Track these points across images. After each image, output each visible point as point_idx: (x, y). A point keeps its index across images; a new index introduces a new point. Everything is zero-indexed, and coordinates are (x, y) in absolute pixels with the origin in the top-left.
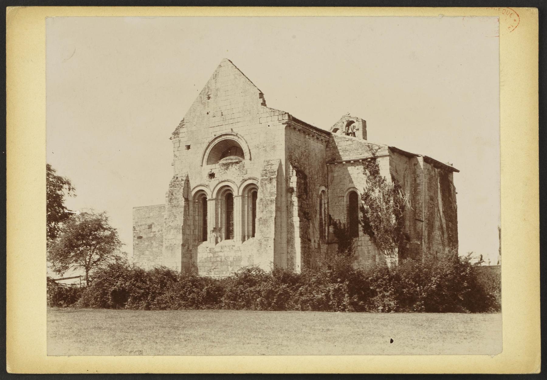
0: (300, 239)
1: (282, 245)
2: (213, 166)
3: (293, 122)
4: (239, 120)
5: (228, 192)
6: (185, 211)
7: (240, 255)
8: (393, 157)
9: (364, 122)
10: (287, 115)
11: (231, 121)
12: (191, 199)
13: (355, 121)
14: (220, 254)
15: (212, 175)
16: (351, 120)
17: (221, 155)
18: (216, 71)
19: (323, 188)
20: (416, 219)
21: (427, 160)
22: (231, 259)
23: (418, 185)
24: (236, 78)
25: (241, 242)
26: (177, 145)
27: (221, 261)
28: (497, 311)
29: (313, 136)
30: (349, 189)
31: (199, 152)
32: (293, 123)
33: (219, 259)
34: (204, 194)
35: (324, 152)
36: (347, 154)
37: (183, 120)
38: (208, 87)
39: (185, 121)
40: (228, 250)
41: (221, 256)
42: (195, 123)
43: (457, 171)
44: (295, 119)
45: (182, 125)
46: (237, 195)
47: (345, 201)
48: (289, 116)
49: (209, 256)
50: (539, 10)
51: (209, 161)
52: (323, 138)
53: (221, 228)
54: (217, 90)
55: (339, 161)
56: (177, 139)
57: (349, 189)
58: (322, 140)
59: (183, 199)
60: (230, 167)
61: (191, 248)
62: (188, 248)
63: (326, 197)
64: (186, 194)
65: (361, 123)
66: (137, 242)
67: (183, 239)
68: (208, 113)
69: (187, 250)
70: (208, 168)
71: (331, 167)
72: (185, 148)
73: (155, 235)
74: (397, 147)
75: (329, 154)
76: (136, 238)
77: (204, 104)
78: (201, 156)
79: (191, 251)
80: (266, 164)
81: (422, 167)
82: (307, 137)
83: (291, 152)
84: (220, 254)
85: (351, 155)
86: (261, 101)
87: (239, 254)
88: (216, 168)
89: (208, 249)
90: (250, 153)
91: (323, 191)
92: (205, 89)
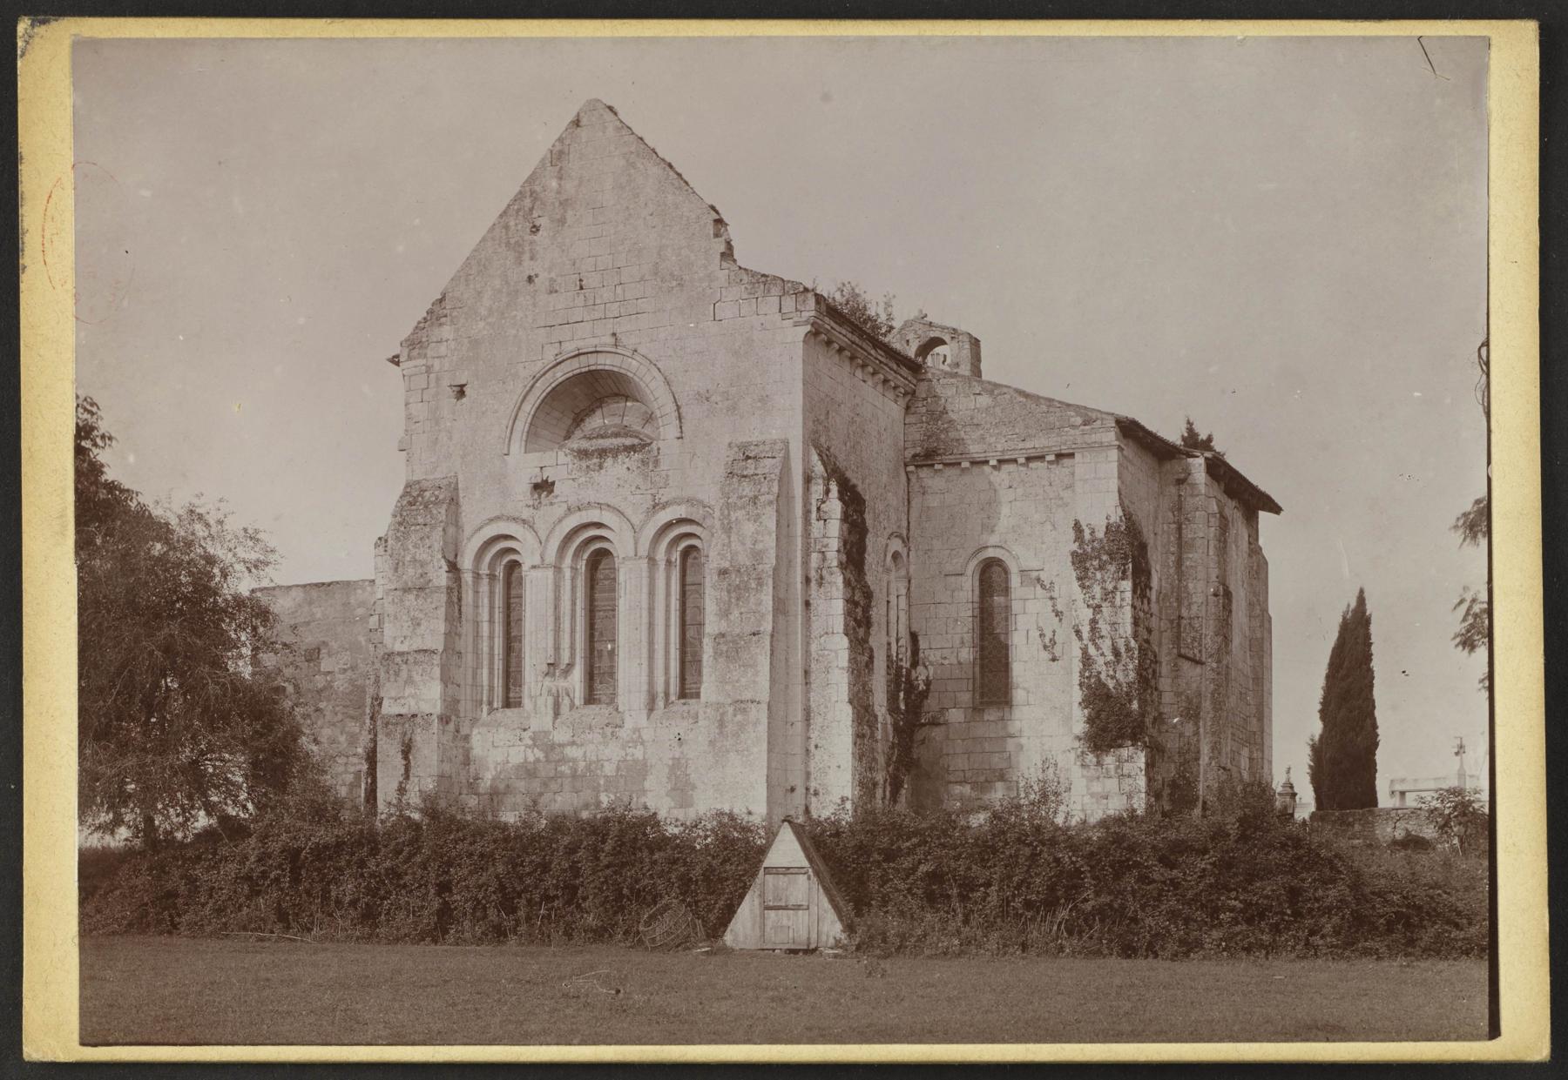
2: (548, 458)
5: (598, 545)
6: (449, 603)
9: (975, 343)
10: (811, 297)
12: (466, 563)
13: (947, 338)
14: (571, 752)
15: (543, 487)
16: (932, 334)
17: (569, 422)
18: (560, 140)
20: (1180, 655)
22: (609, 769)
25: (645, 712)
27: (574, 776)
31: (505, 401)
32: (828, 323)
33: (565, 769)
34: (513, 551)
37: (441, 301)
39: (448, 304)
40: (598, 737)
41: (574, 760)
43: (1275, 509)
46: (537, 561)
47: (968, 587)
48: (819, 299)
50: (1541, 28)
51: (533, 437)
53: (571, 666)
54: (564, 204)
55: (948, 459)
56: (421, 362)
59: (443, 563)
60: (609, 461)
61: (464, 731)
63: (903, 572)
65: (967, 346)
68: (530, 279)
69: (455, 738)
70: (525, 466)
71: (918, 478)
73: (329, 686)
75: (917, 436)
77: (517, 248)
79: (467, 738)
81: (1203, 489)
82: (859, 373)
87: (638, 753)
88: (558, 463)
89: (526, 735)
90: (680, 418)
92: (520, 196)
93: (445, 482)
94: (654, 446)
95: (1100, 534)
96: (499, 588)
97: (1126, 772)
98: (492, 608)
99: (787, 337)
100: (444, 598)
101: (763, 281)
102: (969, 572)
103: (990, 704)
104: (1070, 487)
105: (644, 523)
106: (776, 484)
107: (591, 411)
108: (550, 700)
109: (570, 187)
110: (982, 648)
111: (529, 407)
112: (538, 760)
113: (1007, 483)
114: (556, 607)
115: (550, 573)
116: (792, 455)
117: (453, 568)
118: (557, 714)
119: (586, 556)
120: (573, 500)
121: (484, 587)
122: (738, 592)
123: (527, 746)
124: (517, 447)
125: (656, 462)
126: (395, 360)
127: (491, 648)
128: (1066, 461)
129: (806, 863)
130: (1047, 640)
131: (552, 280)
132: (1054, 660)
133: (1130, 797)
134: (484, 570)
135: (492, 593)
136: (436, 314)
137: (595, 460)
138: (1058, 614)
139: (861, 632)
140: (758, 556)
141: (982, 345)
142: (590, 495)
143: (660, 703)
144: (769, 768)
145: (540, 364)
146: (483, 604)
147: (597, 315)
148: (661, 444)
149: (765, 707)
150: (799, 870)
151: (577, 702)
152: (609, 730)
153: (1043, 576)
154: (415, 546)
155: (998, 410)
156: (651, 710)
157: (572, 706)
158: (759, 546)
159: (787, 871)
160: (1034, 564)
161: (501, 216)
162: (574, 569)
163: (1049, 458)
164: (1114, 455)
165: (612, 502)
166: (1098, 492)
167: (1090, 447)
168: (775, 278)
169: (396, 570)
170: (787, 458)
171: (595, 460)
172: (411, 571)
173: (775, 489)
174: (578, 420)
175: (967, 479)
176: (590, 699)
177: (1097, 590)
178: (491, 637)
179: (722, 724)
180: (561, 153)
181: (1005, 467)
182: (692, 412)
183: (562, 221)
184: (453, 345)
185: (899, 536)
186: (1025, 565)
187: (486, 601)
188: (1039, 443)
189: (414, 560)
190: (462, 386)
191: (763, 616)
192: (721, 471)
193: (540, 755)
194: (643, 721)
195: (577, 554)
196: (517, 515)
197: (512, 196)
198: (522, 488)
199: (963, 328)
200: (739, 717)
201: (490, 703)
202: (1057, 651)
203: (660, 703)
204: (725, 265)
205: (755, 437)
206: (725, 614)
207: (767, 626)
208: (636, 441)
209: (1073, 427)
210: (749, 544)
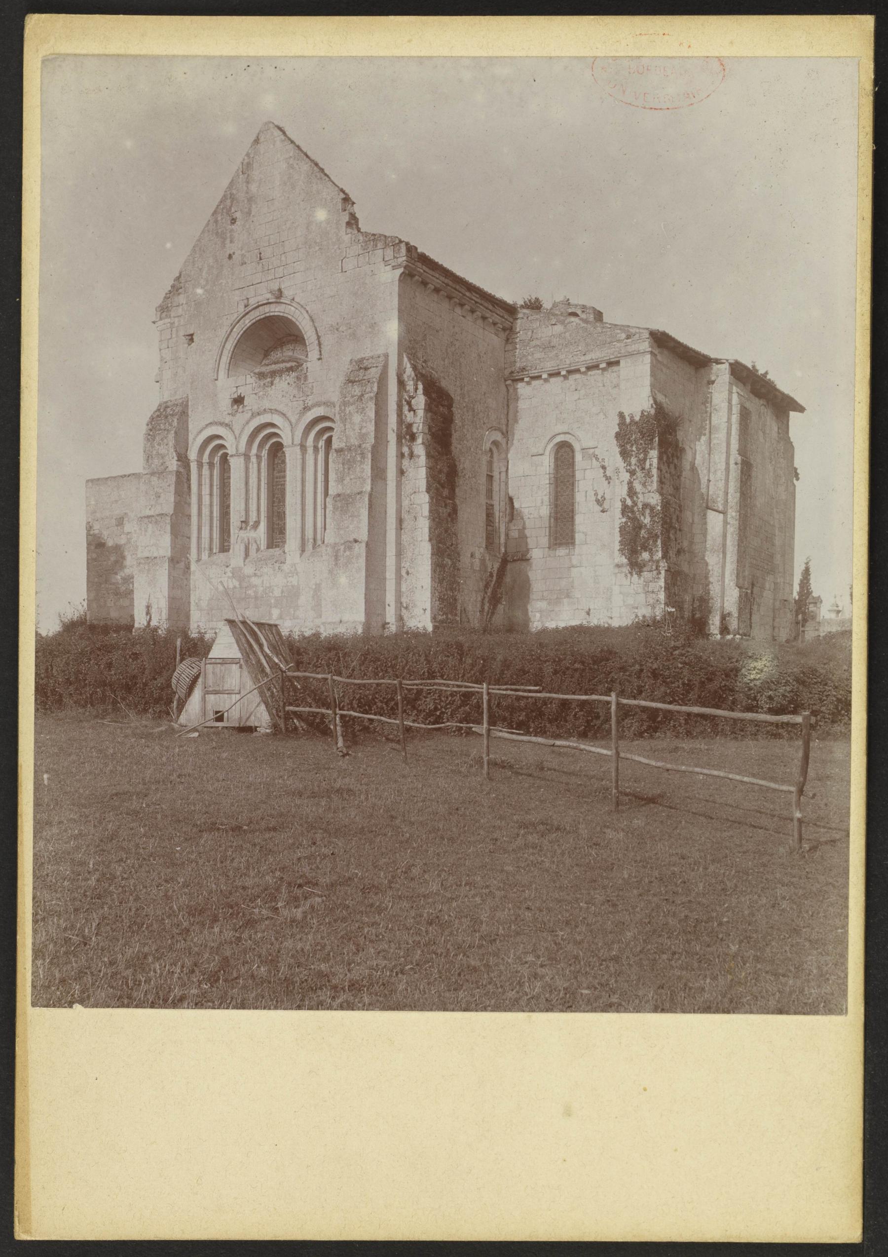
3: (419, 265)
5: (275, 440)
8: (659, 357)
10: (403, 246)
12: (193, 455)
14: (255, 581)
15: (238, 401)
18: (248, 155)
21: (743, 375)
22: (277, 593)
24: (291, 167)
25: (299, 552)
27: (256, 598)
28: (133, 578)
30: (554, 436)
32: (421, 268)
33: (251, 592)
36: (551, 355)
38: (231, 194)
39: (182, 280)
41: (256, 586)
43: (801, 409)
44: (424, 259)
48: (410, 249)
52: (497, 319)
53: (257, 524)
54: (250, 200)
56: (169, 320)
57: (554, 436)
58: (495, 324)
59: (174, 454)
60: (277, 380)
66: (94, 556)
68: (230, 257)
70: (227, 386)
72: (184, 340)
76: (93, 547)
82: (458, 310)
84: (255, 581)
85: (562, 357)
86: (346, 218)
87: (294, 581)
88: (245, 382)
89: (229, 569)
90: (320, 344)
91: (495, 443)
93: (181, 401)
94: (304, 366)
95: (637, 418)
96: (216, 472)
97: (650, 589)
98: (211, 486)
99: (388, 277)
100: (174, 479)
101: (374, 239)
102: (547, 453)
103: (560, 545)
104: (617, 386)
105: (299, 420)
106: (376, 385)
107: (274, 348)
108: (243, 548)
109: (253, 188)
110: (556, 506)
111: (230, 346)
112: (235, 587)
113: (573, 387)
114: (247, 483)
115: (242, 459)
116: (390, 366)
117: (183, 458)
118: (247, 555)
119: (267, 447)
120: (255, 408)
121: (206, 471)
122: (349, 464)
123: (229, 577)
124: (222, 374)
125: (306, 378)
126: (154, 322)
127: (211, 512)
128: (615, 368)
129: (239, 655)
130: (599, 497)
131: (243, 256)
132: (603, 511)
133: (653, 607)
134: (206, 458)
135: (211, 476)
136: (176, 289)
137: (269, 380)
138: (608, 479)
139: (446, 492)
140: (363, 437)
141: (604, 315)
142: (267, 404)
143: (310, 546)
144: (366, 588)
145: (236, 315)
146: (203, 485)
147: (270, 278)
148: (309, 364)
149: (364, 545)
150: (233, 661)
151: (262, 548)
152: (277, 565)
153: (597, 452)
154: (159, 444)
155: (567, 334)
156: (303, 551)
157: (258, 550)
158: (364, 431)
159: (224, 662)
160: (591, 444)
161: (213, 215)
162: (259, 457)
163: (603, 365)
164: (648, 358)
165: (281, 408)
166: (635, 390)
167: (631, 355)
168: (381, 235)
169: (148, 461)
170: (385, 367)
171: (269, 380)
172: (156, 461)
173: (375, 389)
174: (266, 354)
175: (547, 386)
176: (271, 545)
177: (634, 460)
178: (211, 505)
179: (336, 558)
180: (249, 164)
181: (572, 377)
182: (328, 341)
183: (249, 213)
184: (185, 307)
185: (499, 430)
186: (585, 445)
187: (208, 481)
188: (595, 355)
189: (158, 454)
190: (192, 335)
191: (364, 480)
192: (342, 379)
193: (237, 584)
194: (297, 559)
195: (261, 446)
196: (222, 420)
197: (219, 200)
198: (225, 402)
199: (588, 304)
200: (348, 553)
201: (211, 549)
202: (606, 505)
203: (310, 546)
204: (349, 230)
205: (367, 354)
206: (340, 480)
207: (368, 488)
208: (294, 364)
209: (619, 341)
210: (357, 431)
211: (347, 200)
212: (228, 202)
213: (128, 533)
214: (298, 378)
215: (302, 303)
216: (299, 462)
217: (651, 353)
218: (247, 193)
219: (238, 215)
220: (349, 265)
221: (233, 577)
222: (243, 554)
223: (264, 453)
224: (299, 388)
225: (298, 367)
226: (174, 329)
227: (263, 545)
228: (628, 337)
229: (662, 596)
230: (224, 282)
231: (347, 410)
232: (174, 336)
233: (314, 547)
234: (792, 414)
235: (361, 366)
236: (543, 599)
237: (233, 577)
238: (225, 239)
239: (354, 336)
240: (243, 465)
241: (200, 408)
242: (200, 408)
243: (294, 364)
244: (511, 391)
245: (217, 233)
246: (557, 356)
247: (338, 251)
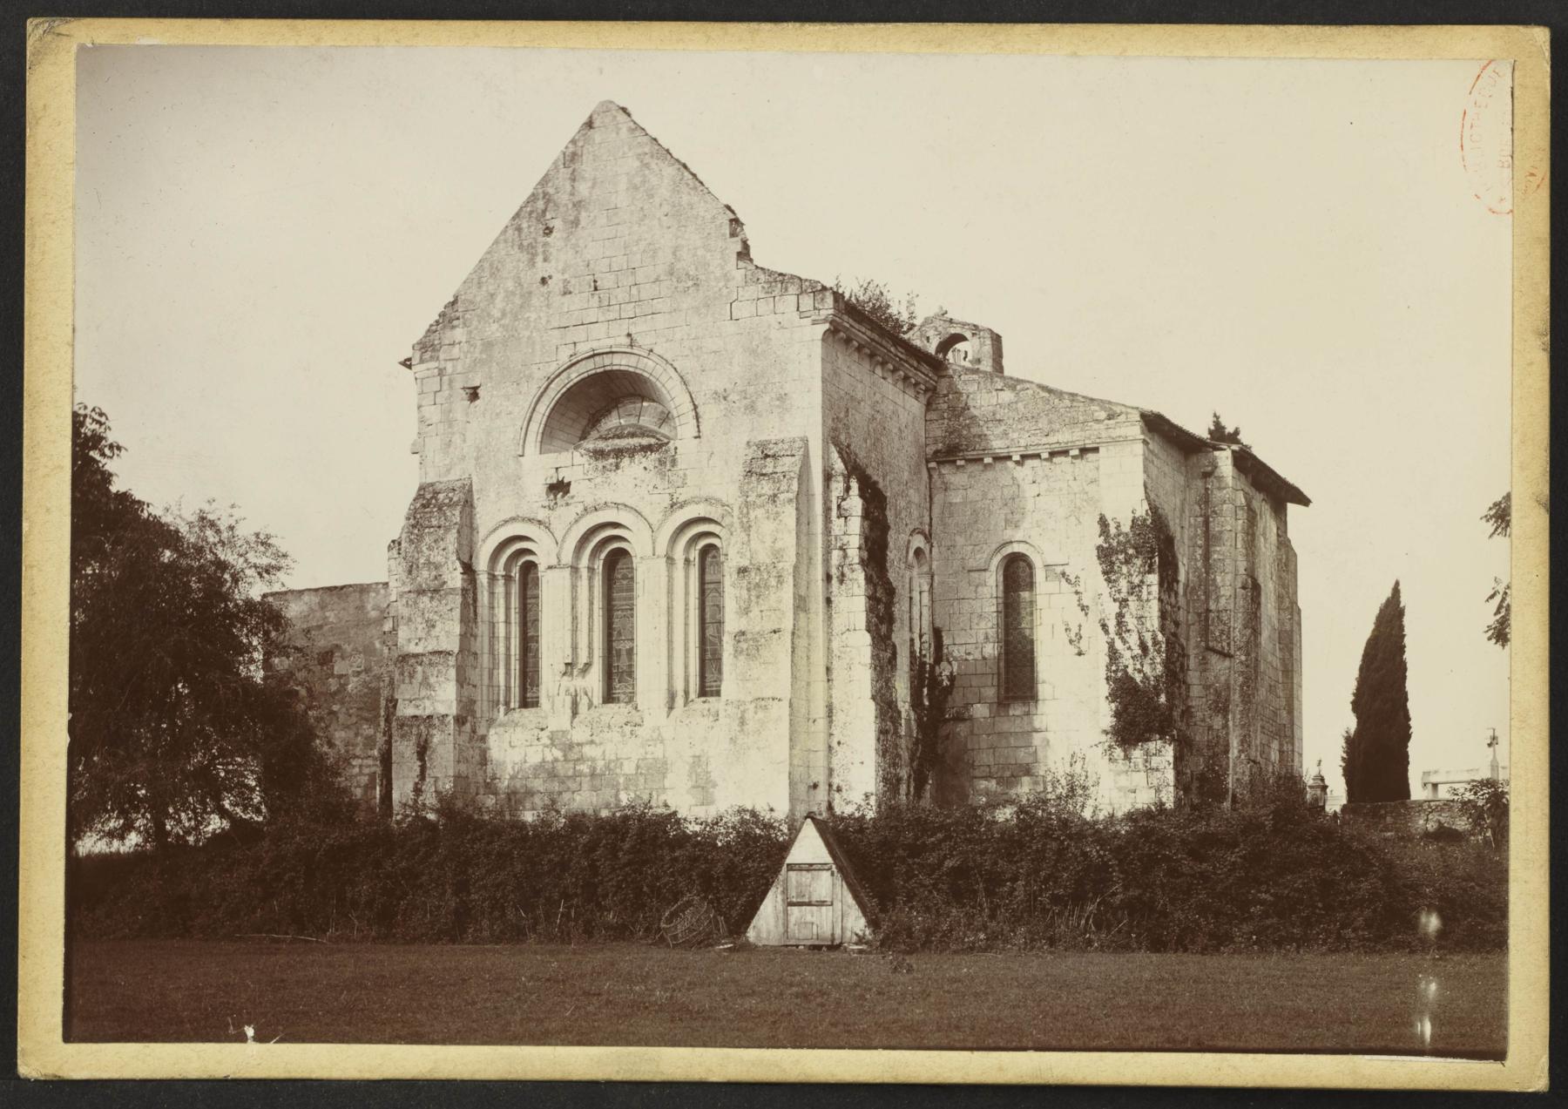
0: (872, 706)
1: (809, 720)
2: (564, 458)
3: (846, 317)
4: (658, 305)
5: (615, 545)
7: (659, 754)
9: (997, 340)
11: (628, 311)
12: (482, 564)
13: (968, 334)
14: (588, 751)
15: (559, 488)
17: (584, 422)
18: (573, 142)
19: (918, 542)
22: (629, 768)
23: (1218, 539)
26: (434, 384)
27: (593, 775)
29: (894, 371)
31: (517, 406)
32: (847, 322)
33: (584, 768)
35: (920, 425)
37: (453, 303)
38: (545, 194)
39: (460, 307)
41: (593, 760)
42: (496, 313)
43: (1304, 500)
45: (448, 317)
48: (838, 297)
49: (549, 758)
53: (588, 665)
54: (578, 205)
55: (971, 454)
59: (458, 564)
60: (626, 461)
62: (474, 732)
63: (925, 569)
64: (466, 549)
65: (988, 342)
67: (459, 701)
68: (544, 281)
69: (471, 739)
70: (540, 467)
71: (940, 474)
74: (1168, 416)
75: (939, 433)
77: (530, 250)
78: (521, 423)
80: (753, 452)
81: (1230, 481)
82: (879, 371)
83: (837, 419)
88: (574, 463)
90: (697, 417)
92: (533, 198)
96: (515, 589)
98: (508, 609)
100: (459, 599)
102: (993, 567)
107: (605, 412)
108: (569, 700)
109: (583, 189)
111: (544, 408)
112: (556, 760)
113: (1030, 478)
115: (567, 572)
116: (811, 454)
117: (469, 569)
118: (575, 713)
119: (603, 556)
120: (589, 502)
121: (500, 589)
125: (674, 462)
126: (407, 363)
127: (508, 649)
128: (1090, 456)
132: (1080, 654)
134: (500, 570)
137: (611, 461)
138: (1083, 608)
140: (778, 555)
143: (680, 700)
146: (499, 608)
148: (678, 443)
149: (786, 703)
152: (628, 729)
156: (671, 708)
157: (590, 705)
158: (779, 545)
162: (591, 570)
164: (1139, 448)
166: (1123, 484)
167: (1115, 441)
168: (793, 277)
169: (410, 572)
172: (425, 574)
173: (795, 487)
174: (594, 421)
175: (989, 474)
176: (609, 698)
178: (508, 638)
179: (742, 722)
180: (574, 154)
181: (1029, 463)
182: (710, 412)
183: (576, 223)
184: (465, 347)
185: (922, 533)
187: (502, 602)
188: (1063, 437)
189: (429, 563)
190: (475, 388)
192: (738, 470)
193: (558, 754)
202: (1083, 645)
203: (680, 700)
204: (741, 264)
207: (787, 624)
208: (653, 441)
209: (1097, 421)
211: (736, 222)
212: (540, 204)
213: (341, 676)
214: (661, 462)
215: (668, 357)
216: (664, 580)
217: (1144, 442)
218: (572, 194)
219: (557, 224)
220: (743, 310)
221: (553, 744)
222: (569, 712)
223: (599, 565)
224: (662, 475)
225: (661, 446)
226: (445, 379)
227: (597, 697)
228: (1110, 418)
229: (1170, 775)
230: (533, 316)
231: (752, 515)
232: (445, 387)
233: (686, 704)
234: (1292, 508)
235: (766, 453)
236: (987, 777)
237: (553, 744)
238: (534, 255)
239: (751, 408)
240: (568, 583)
241: (493, 495)
242: (493, 495)
243: (653, 441)
244: (935, 476)
245: (521, 247)
246: (1005, 434)
247: (725, 291)
